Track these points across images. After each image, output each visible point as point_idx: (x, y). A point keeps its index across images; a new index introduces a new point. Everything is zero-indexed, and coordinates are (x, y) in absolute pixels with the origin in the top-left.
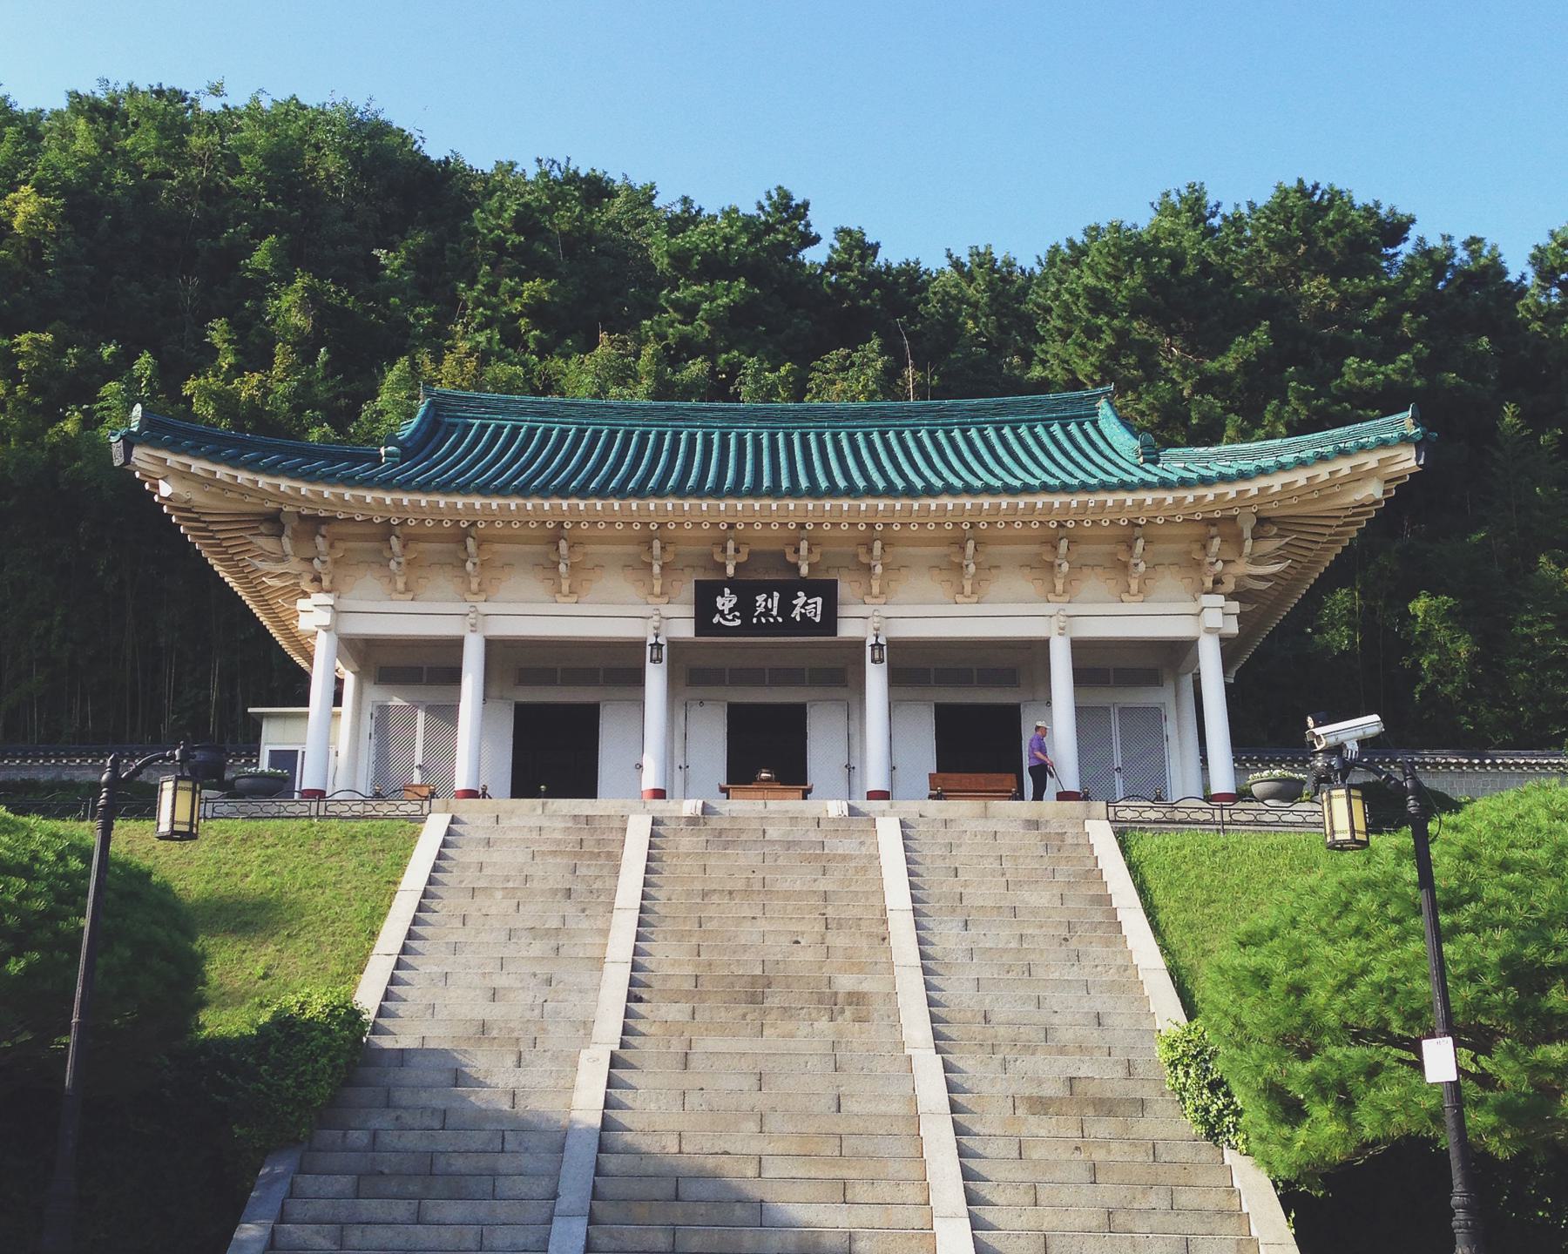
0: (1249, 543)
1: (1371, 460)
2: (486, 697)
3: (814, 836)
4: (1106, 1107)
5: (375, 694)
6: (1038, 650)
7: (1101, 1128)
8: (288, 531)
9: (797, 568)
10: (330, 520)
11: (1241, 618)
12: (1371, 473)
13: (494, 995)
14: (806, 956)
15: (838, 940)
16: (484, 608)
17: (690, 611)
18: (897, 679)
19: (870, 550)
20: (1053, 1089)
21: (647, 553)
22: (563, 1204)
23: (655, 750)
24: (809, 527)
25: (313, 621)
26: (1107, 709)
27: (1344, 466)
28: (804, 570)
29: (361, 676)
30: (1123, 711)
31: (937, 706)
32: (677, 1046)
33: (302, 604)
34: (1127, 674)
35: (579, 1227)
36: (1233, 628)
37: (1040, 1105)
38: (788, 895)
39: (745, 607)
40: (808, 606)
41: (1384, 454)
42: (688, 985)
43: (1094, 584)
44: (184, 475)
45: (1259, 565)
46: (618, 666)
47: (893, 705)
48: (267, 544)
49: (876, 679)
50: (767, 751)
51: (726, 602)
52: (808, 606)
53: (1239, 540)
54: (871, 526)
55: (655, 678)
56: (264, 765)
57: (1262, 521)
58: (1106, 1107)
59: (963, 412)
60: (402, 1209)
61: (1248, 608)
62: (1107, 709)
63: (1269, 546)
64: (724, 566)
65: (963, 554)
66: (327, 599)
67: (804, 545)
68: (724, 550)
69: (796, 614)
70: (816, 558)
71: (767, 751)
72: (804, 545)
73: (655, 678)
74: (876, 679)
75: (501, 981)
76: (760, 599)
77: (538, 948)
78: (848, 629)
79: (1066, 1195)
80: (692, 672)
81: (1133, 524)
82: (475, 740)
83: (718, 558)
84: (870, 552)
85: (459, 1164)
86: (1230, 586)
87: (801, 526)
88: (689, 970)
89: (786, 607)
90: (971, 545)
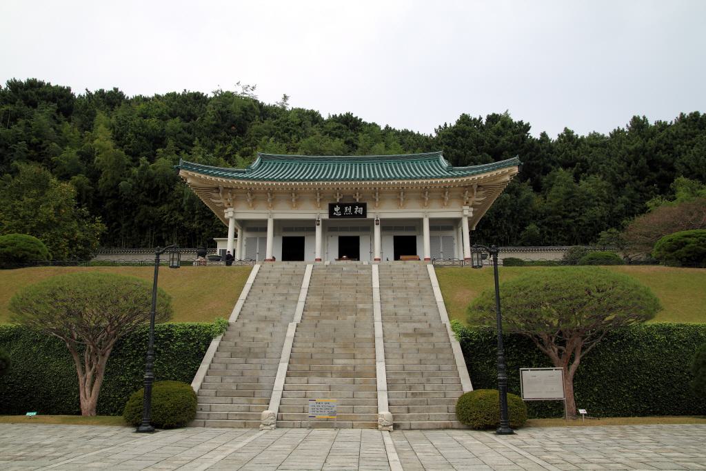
0: (475, 192)
1: (507, 170)
2: (274, 235)
3: (356, 270)
4: (423, 335)
5: (246, 235)
6: (420, 221)
7: (422, 340)
8: (221, 191)
9: (356, 200)
10: (231, 189)
11: (473, 212)
12: (507, 173)
13: (269, 309)
14: (350, 300)
15: (359, 295)
16: (273, 211)
17: (327, 212)
18: (383, 229)
19: (375, 195)
20: (410, 331)
21: (318, 195)
22: (282, 359)
23: (319, 248)
24: (405, 188)
25: (232, 215)
26: (439, 237)
27: (500, 172)
28: (358, 200)
29: (242, 230)
30: (443, 237)
31: (394, 237)
32: (315, 322)
33: (225, 211)
34: (443, 227)
35: (286, 364)
36: (471, 215)
37: (406, 335)
38: (348, 285)
39: (342, 210)
40: (359, 210)
41: (510, 168)
42: (319, 307)
43: (435, 204)
44: (193, 177)
45: (478, 198)
46: (309, 226)
47: (381, 237)
48: (215, 195)
49: (377, 230)
50: (349, 249)
51: (337, 209)
52: (359, 210)
53: (473, 192)
54: (375, 188)
55: (319, 230)
56: (218, 253)
57: (479, 186)
58: (423, 335)
59: (368, 159)
60: (242, 361)
61: (476, 210)
62: (439, 237)
63: (481, 193)
64: (336, 199)
65: (401, 195)
66: (232, 209)
67: (357, 194)
68: (336, 195)
69: (356, 212)
70: (361, 197)
71: (349, 249)
72: (357, 194)
73: (319, 230)
74: (377, 230)
75: (272, 306)
76: (346, 208)
77: (281, 298)
78: (369, 216)
79: (411, 356)
80: (328, 228)
81: (445, 187)
82: (272, 247)
83: (335, 197)
84: (377, 195)
85: (257, 350)
86: (471, 204)
87: (356, 188)
88: (320, 303)
89: (353, 210)
90: (402, 193)
